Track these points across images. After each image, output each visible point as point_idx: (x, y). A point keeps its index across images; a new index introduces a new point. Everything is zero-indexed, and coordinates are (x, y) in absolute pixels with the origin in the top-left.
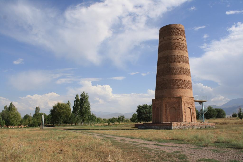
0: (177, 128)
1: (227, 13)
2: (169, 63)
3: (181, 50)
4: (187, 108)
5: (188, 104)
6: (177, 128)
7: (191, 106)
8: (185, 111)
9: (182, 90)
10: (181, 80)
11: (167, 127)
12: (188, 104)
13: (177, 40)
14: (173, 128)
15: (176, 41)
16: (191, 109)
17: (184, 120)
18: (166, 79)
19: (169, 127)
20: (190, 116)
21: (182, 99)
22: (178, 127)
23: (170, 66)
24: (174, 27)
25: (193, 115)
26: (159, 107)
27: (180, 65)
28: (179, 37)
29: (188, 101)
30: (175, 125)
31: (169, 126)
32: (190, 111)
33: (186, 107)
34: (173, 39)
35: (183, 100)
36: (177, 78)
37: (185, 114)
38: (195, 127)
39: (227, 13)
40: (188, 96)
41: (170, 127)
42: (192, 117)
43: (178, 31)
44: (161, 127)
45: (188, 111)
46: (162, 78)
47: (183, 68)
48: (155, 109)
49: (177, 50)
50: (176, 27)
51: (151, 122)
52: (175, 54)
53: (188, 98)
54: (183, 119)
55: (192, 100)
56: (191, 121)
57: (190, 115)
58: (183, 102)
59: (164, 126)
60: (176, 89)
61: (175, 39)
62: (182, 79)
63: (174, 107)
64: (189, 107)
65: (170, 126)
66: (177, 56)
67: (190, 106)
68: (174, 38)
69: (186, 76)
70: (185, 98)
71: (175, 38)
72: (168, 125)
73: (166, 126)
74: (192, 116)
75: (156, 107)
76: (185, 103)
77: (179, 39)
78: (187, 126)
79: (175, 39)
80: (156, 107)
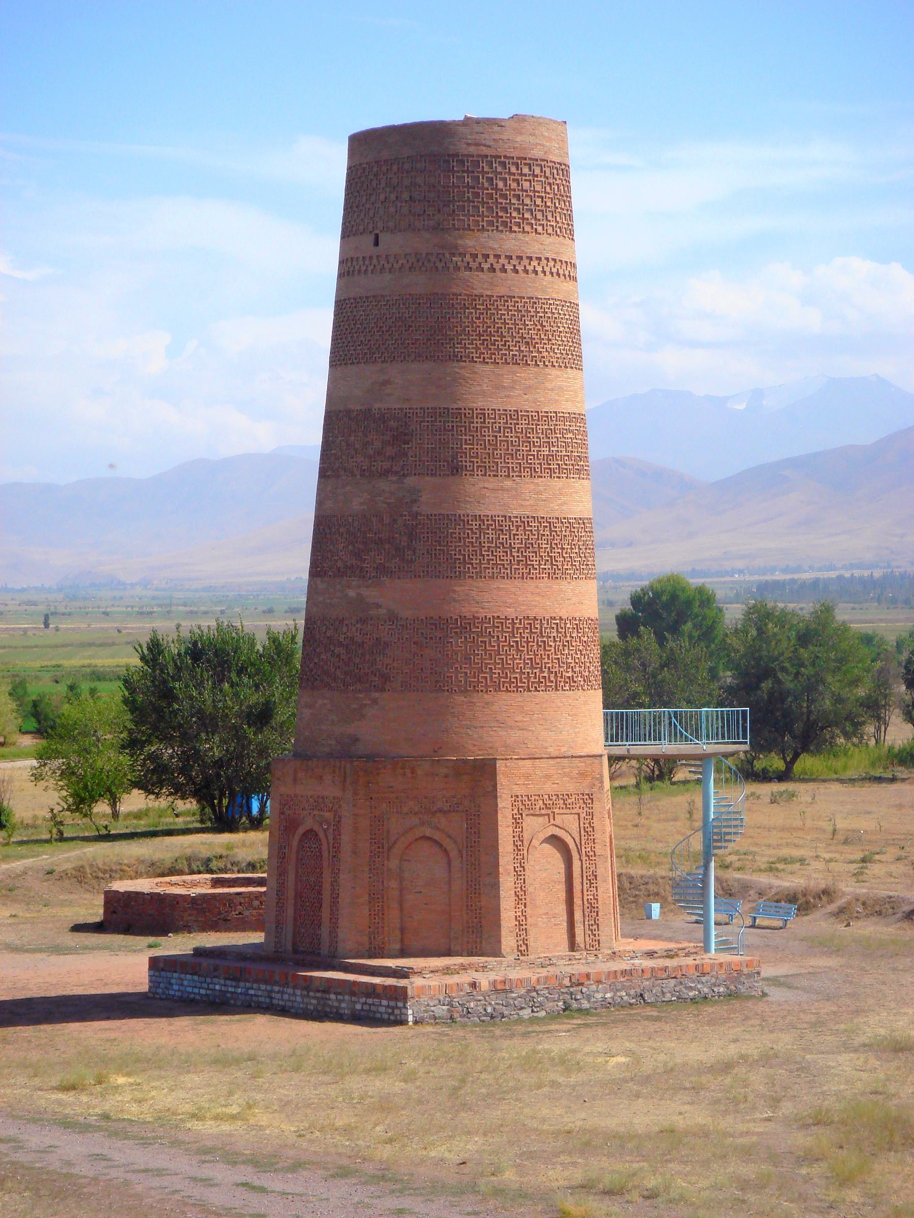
0: (441, 1011)
1: (256, 938)
2: (410, 481)
3: (521, 361)
4: (535, 843)
5: (548, 811)
6: (441, 1011)
7: (574, 827)
8: (520, 872)
9: (504, 702)
10: (500, 622)
11: (370, 1001)
12: (548, 808)
13: (492, 269)
14: (410, 1012)
15: (480, 283)
16: (572, 846)
17: (508, 941)
18: (382, 611)
19: (384, 1002)
20: (562, 909)
21: (501, 780)
22: (450, 1004)
23: (414, 501)
24: (472, 150)
25: (588, 896)
26: (321, 835)
27: (501, 497)
28: (510, 243)
29: (549, 788)
30: (430, 979)
31: (389, 999)
32: (561, 867)
33: (526, 836)
34: (457, 269)
35: (509, 785)
36: (467, 610)
37: (521, 897)
38: (588, 998)
39: (256, 938)
40: (552, 751)
41: (392, 1003)
42: (578, 915)
43: (501, 185)
44: (333, 996)
45: (545, 866)
46: (352, 593)
47: (524, 523)
48: (295, 843)
49: (479, 367)
50: (485, 151)
51: (263, 934)
52: (460, 404)
53: (551, 762)
54: (504, 932)
55: (582, 775)
56: (565, 944)
57: (563, 895)
58: (504, 804)
59: (353, 994)
60: (460, 699)
61: (486, 266)
62: (511, 612)
63: (435, 841)
64: (555, 840)
65: (396, 999)
66: (477, 423)
67: (568, 825)
68: (475, 256)
69: (544, 584)
70: (528, 763)
71: (475, 256)
72: (379, 991)
73: (368, 996)
74: (577, 901)
75: (301, 830)
76: (525, 806)
77: (503, 261)
78: (523, 991)
79: (474, 265)
80: (301, 830)
